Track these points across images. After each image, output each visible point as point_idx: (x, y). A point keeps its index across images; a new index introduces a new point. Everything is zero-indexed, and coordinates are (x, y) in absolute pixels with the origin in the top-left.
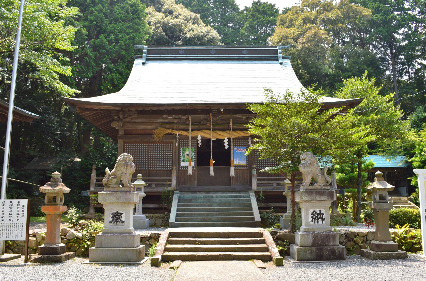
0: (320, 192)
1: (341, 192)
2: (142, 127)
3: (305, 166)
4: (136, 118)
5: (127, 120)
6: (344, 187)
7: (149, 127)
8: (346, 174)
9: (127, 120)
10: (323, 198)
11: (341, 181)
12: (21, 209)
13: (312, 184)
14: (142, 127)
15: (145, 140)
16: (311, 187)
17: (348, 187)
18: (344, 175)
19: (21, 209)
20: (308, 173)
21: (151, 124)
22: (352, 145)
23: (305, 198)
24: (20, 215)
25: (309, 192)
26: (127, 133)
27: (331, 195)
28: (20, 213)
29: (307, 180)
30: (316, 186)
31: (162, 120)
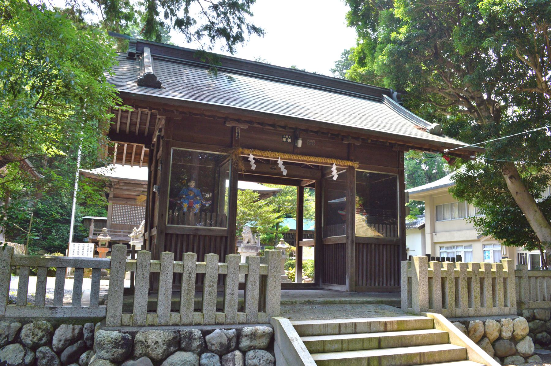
0: (251, 248)
1: (262, 248)
2: (127, 193)
3: (245, 233)
4: (123, 186)
5: (116, 187)
6: (265, 245)
7: (133, 193)
8: (267, 235)
9: (116, 187)
10: (253, 251)
11: (264, 240)
12: (89, 249)
13: (248, 242)
14: (127, 193)
15: (129, 203)
16: (247, 245)
17: (268, 245)
18: (265, 236)
19: (89, 249)
20: (246, 237)
21: (135, 191)
22: (270, 223)
23: (244, 250)
24: (89, 252)
25: (246, 247)
26: (115, 197)
27: (257, 250)
28: (89, 251)
29: (246, 241)
30: (250, 244)
31: (142, 189)
